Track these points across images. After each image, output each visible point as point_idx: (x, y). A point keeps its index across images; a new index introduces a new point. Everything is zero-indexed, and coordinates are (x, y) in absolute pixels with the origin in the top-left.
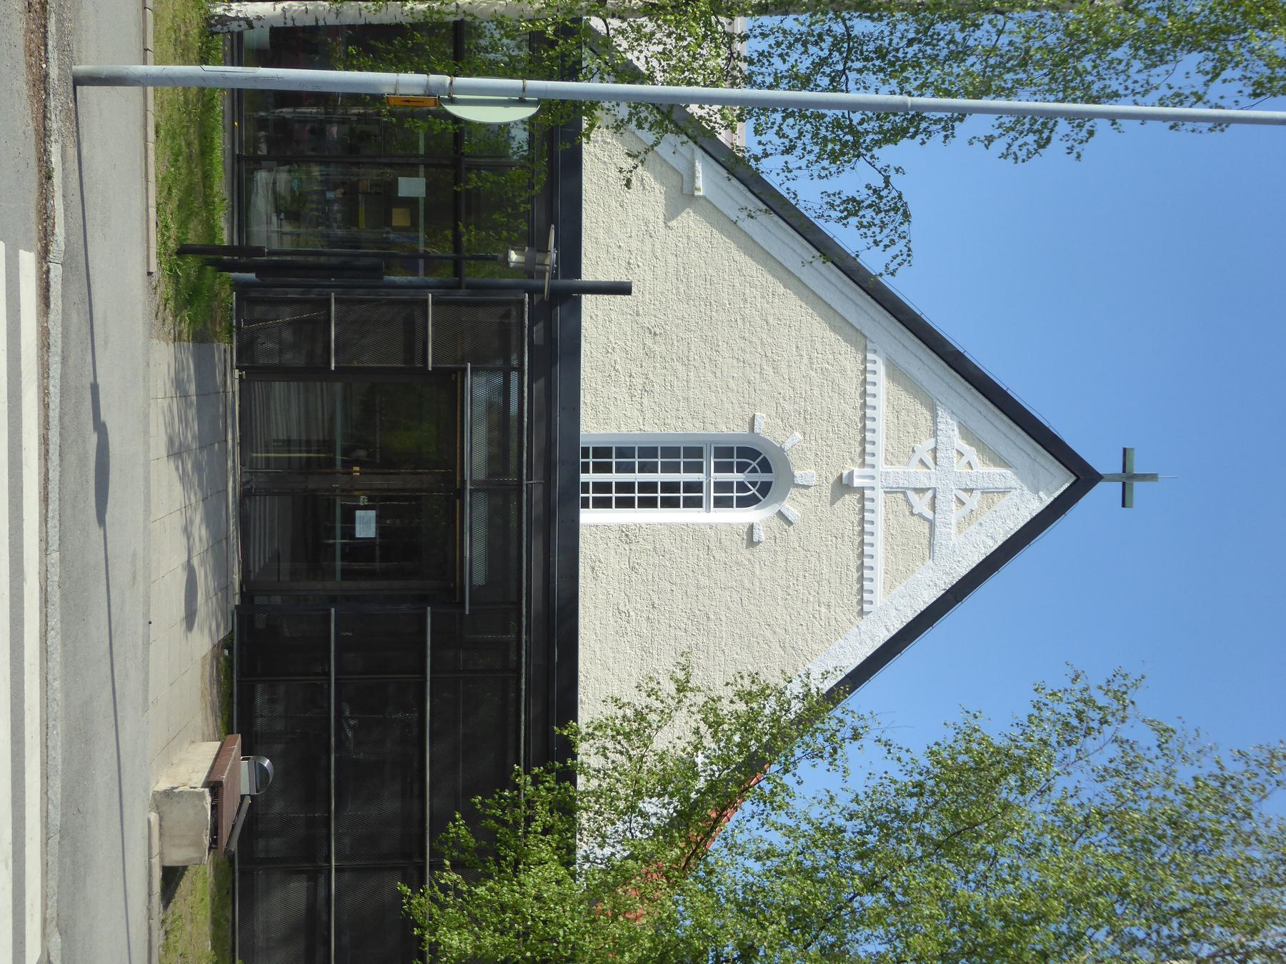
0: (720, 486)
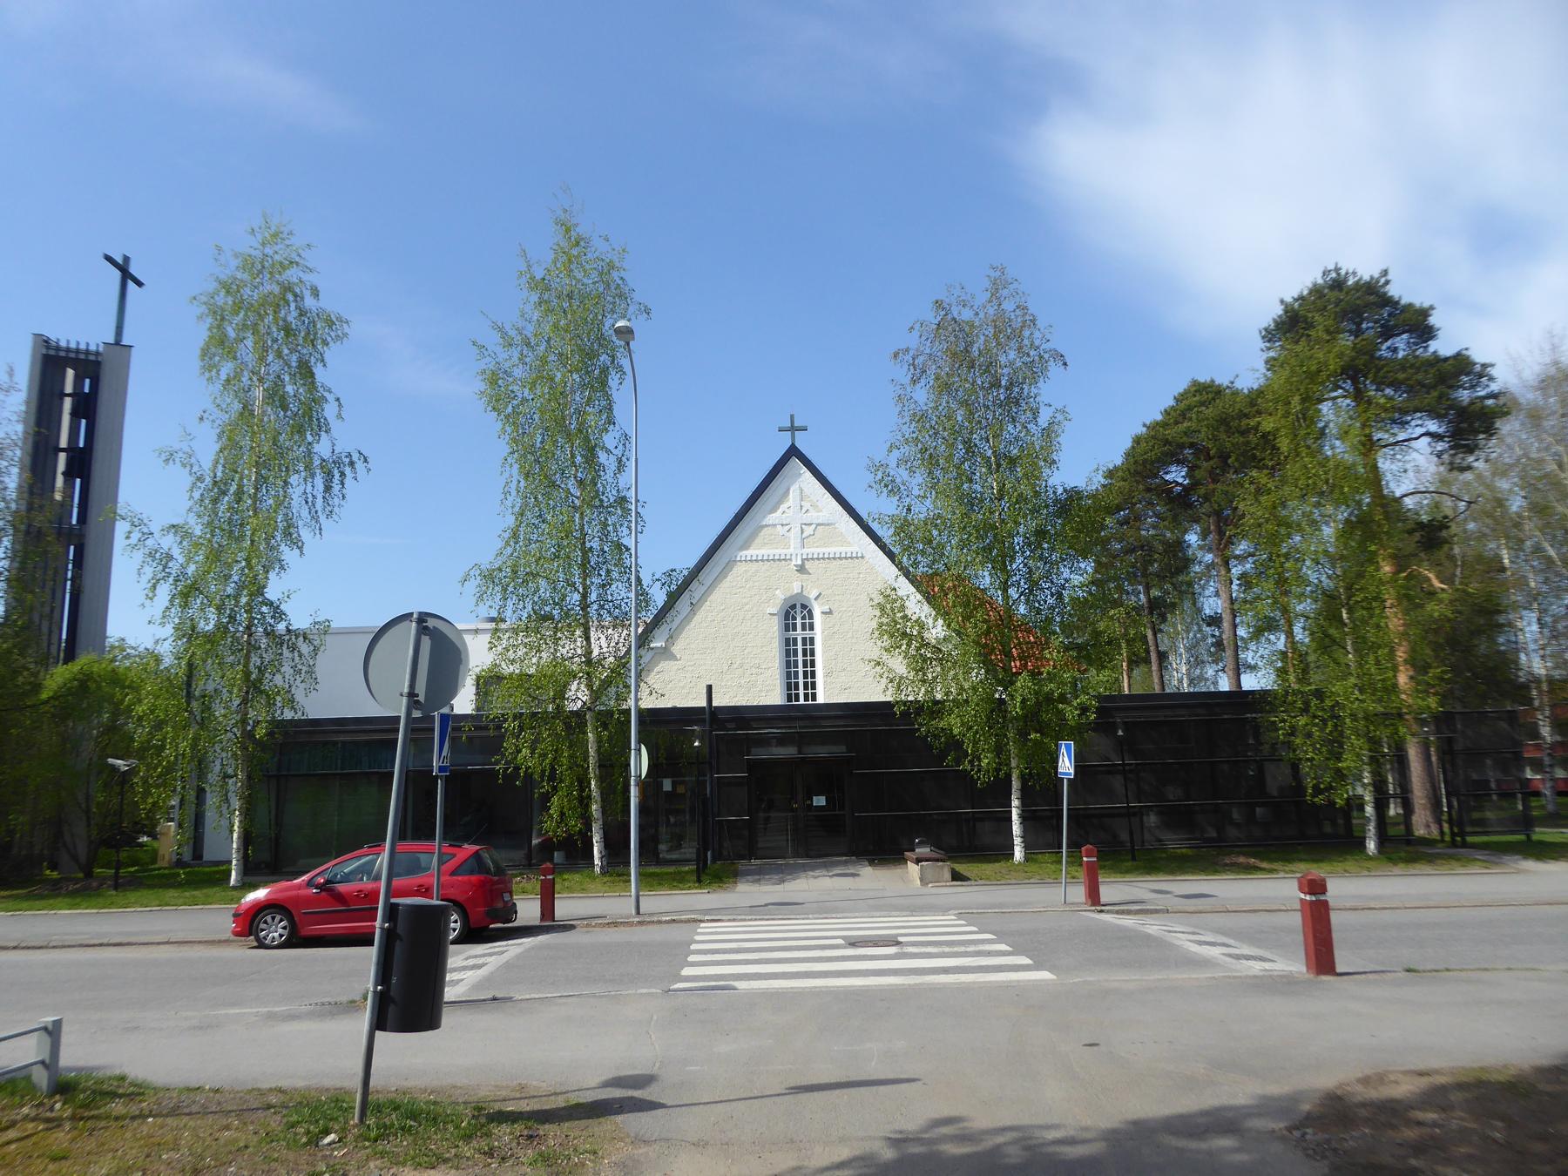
0: (804, 629)
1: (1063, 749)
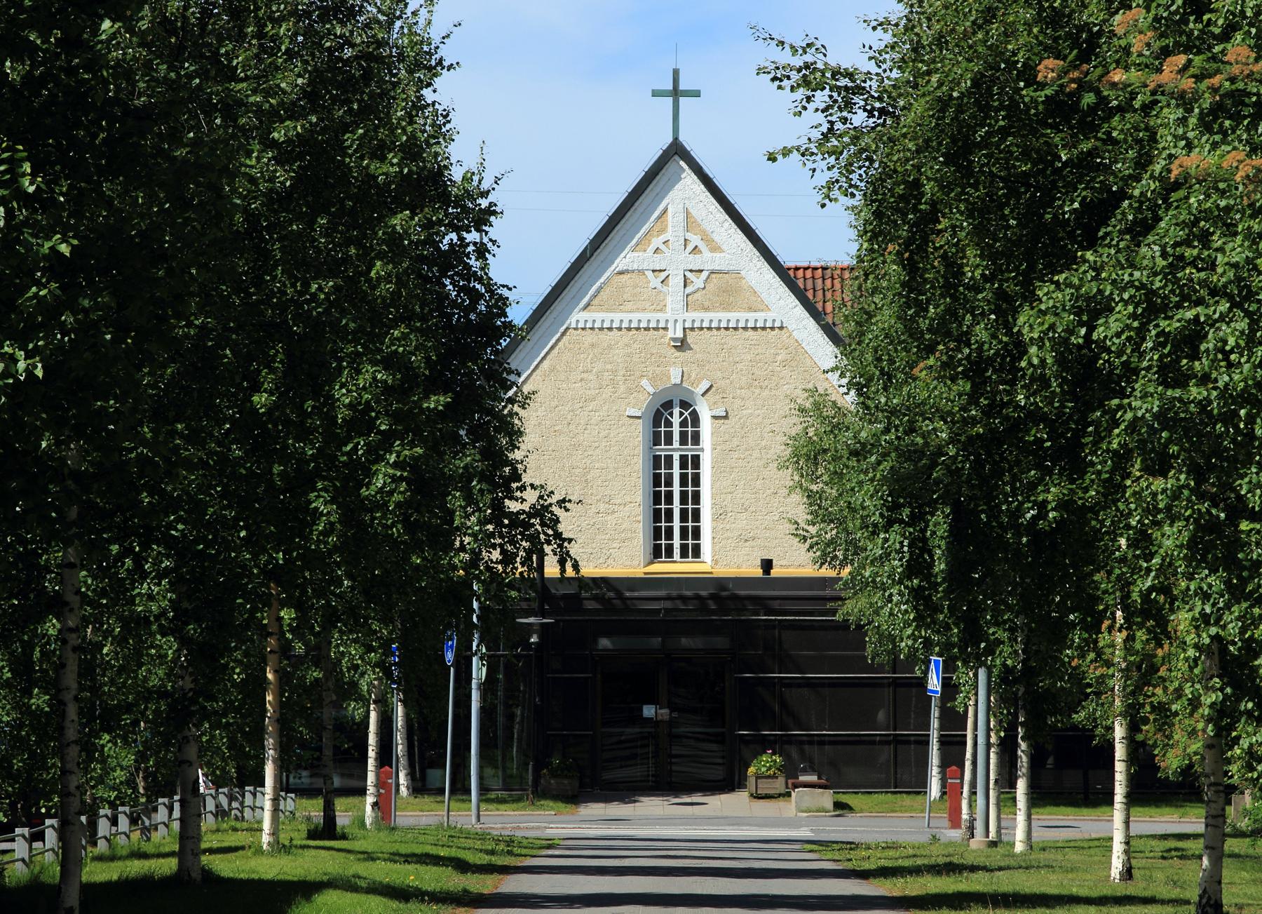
1: (932, 666)
